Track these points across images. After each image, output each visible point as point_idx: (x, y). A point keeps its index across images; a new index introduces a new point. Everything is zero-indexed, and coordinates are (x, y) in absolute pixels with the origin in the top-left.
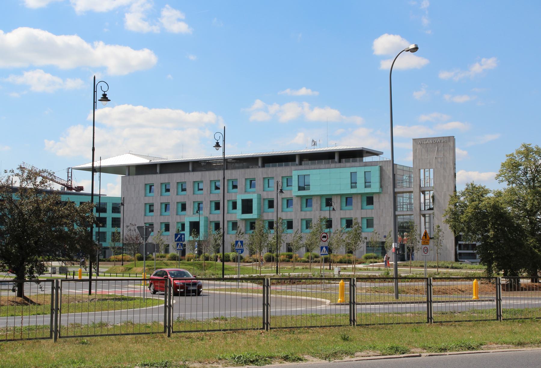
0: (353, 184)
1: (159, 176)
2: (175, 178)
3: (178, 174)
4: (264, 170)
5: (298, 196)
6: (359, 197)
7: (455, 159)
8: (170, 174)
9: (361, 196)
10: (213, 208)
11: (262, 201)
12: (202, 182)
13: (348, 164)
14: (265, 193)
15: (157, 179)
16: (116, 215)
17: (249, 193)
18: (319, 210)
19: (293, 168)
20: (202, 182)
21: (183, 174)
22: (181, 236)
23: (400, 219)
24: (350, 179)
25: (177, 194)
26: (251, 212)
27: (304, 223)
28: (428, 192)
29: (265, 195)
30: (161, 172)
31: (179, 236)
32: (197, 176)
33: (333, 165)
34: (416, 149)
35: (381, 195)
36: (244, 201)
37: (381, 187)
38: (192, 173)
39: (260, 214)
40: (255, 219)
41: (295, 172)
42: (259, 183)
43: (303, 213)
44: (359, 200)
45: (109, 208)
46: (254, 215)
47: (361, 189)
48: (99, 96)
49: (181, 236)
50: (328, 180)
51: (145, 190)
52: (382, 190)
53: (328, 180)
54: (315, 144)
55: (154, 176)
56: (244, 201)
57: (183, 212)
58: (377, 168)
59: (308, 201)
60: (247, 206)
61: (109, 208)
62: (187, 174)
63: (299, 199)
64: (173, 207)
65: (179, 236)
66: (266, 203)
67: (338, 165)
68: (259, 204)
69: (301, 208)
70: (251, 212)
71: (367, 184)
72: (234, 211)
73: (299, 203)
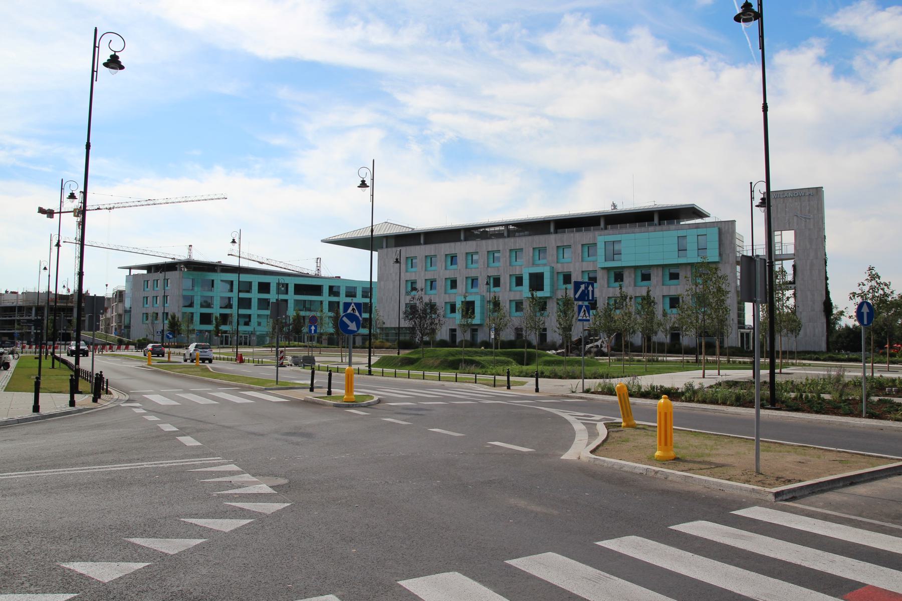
0: (682, 250)
1: (423, 247)
2: (460, 248)
3: (447, 245)
4: (559, 236)
7: (791, 512)
8: (437, 245)
10: (514, 283)
11: (556, 275)
12: (477, 253)
14: (559, 265)
16: (526, 281)
17: (538, 265)
19: (597, 233)
20: (435, 256)
21: (452, 244)
22: (586, 288)
25: (446, 269)
26: (542, 290)
29: (559, 268)
30: (425, 243)
31: (583, 287)
32: (430, 249)
33: (651, 228)
36: (532, 276)
37: (720, 255)
38: (464, 243)
39: (554, 290)
40: (547, 298)
41: (601, 237)
42: (461, 260)
43: (611, 290)
45: (343, 292)
46: (546, 293)
47: (692, 257)
48: (104, 56)
49: (586, 288)
50: (637, 248)
53: (637, 248)
54: (614, 206)
55: (418, 247)
56: (532, 276)
57: (454, 291)
58: (716, 230)
59: (618, 275)
60: (537, 281)
61: (343, 292)
62: (458, 244)
63: (605, 272)
64: (440, 284)
65: (583, 287)
66: (561, 278)
67: (658, 228)
68: (552, 278)
69: (608, 283)
70: (542, 290)
71: (701, 249)
72: (519, 288)
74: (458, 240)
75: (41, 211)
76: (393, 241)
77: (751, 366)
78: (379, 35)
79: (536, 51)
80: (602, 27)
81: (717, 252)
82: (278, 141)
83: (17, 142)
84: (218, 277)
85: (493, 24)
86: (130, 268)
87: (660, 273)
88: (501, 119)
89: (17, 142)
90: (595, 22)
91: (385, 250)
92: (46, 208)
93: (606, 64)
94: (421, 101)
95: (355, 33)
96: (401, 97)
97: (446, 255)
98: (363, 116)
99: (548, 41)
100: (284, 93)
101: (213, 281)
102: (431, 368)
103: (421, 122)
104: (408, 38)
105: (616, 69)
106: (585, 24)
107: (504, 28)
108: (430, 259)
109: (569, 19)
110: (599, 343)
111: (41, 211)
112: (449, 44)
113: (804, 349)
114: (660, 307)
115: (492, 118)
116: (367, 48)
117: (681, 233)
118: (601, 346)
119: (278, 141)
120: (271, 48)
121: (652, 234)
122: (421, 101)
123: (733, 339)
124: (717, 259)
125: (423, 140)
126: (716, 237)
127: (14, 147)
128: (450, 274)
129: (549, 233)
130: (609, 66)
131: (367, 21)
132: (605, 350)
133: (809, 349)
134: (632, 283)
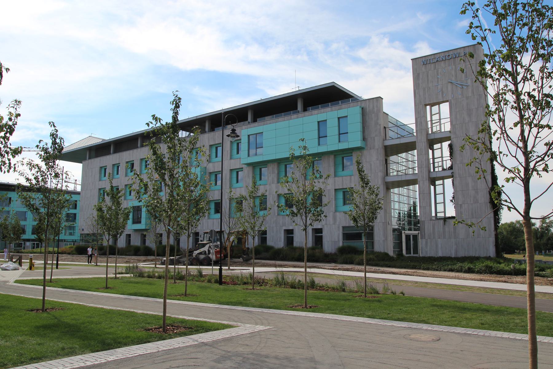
0: (321, 136)
4: (212, 134)
5: (249, 165)
6: (332, 157)
9: (335, 155)
13: (315, 112)
14: (211, 165)
15: (109, 160)
18: (276, 182)
23: (219, 215)
24: (317, 132)
27: (340, 195)
28: (441, 182)
30: (115, 152)
34: (418, 74)
35: (365, 152)
37: (364, 139)
44: (332, 164)
47: (332, 144)
50: (281, 137)
51: (100, 173)
52: (366, 145)
63: (250, 169)
73: (251, 175)
76: (93, 153)
78: (255, 52)
79: (357, 60)
80: (397, 43)
81: (359, 136)
84: (13, 195)
85: (327, 44)
90: (392, 41)
91: (87, 162)
99: (362, 53)
101: (10, 198)
106: (386, 41)
107: (334, 46)
108: (117, 166)
109: (375, 39)
110: (206, 248)
113: (467, 254)
120: (188, 63)
123: (384, 243)
124: (358, 144)
126: (359, 118)
132: (213, 257)
133: (472, 254)
134: (276, 179)
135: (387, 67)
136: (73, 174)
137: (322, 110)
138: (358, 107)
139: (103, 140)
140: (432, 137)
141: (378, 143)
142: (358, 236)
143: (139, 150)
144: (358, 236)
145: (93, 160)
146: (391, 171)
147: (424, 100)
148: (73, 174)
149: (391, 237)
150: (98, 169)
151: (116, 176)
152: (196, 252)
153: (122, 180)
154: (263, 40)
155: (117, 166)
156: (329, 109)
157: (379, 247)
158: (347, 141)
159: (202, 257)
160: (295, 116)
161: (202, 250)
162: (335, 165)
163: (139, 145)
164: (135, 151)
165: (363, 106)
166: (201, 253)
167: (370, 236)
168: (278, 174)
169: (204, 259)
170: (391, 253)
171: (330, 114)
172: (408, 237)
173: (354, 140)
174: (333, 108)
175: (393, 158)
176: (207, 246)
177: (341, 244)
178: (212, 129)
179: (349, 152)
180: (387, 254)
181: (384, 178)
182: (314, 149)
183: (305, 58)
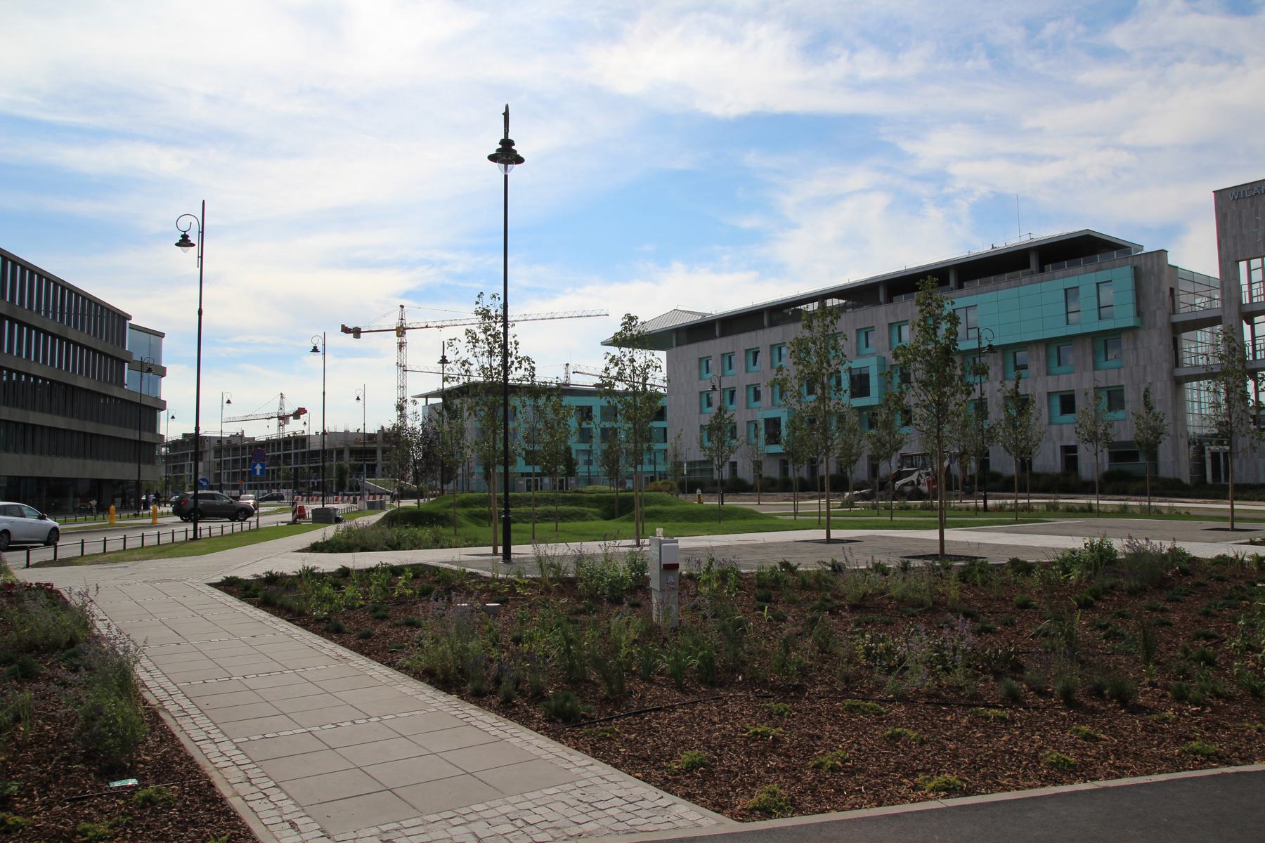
3: (747, 335)
4: (891, 307)
6: (1089, 340)
8: (735, 337)
13: (1060, 273)
15: (714, 347)
17: (864, 356)
25: (747, 371)
26: (867, 394)
30: (723, 335)
35: (1141, 333)
37: (1139, 313)
44: (1089, 351)
47: (1087, 323)
55: (712, 342)
70: (867, 394)
74: (760, 326)
75: (345, 330)
77: (1236, 515)
78: (871, 65)
79: (1104, 54)
81: (1130, 310)
82: (749, 223)
83: (448, 256)
85: (1032, 26)
86: (427, 396)
87: (1042, 354)
88: (1054, 159)
89: (448, 256)
91: (674, 350)
92: (350, 326)
93: (1217, 55)
94: (937, 148)
95: (838, 68)
96: (908, 147)
97: (747, 351)
98: (858, 178)
99: (1119, 36)
100: (752, 158)
102: (71, 514)
103: (939, 177)
104: (912, 63)
105: (1235, 59)
107: (1051, 28)
108: (728, 357)
110: (914, 478)
111: (345, 330)
112: (969, 64)
114: (1042, 414)
115: (1042, 159)
116: (856, 85)
117: (1070, 282)
118: (919, 483)
119: (749, 223)
121: (1025, 290)
122: (937, 148)
123: (1174, 461)
124: (1130, 322)
125: (944, 201)
127: (444, 263)
128: (750, 379)
129: (878, 303)
130: (1226, 57)
131: (853, 50)
132: (925, 489)
135: (1180, 60)
136: (656, 368)
137: (1071, 271)
138: (1128, 268)
139: (704, 315)
140: (1249, 309)
141: (1161, 319)
142: (1133, 456)
143: (767, 331)
144: (1133, 456)
145: (684, 347)
146: (1186, 355)
147: (1232, 249)
148: (656, 368)
149: (1187, 454)
150: (695, 362)
151: (728, 372)
152: (899, 483)
153: (739, 377)
154: (889, 36)
155: (728, 357)
156: (1080, 269)
157: (1165, 471)
158: (1111, 317)
159: (908, 489)
160: (1026, 280)
161: (908, 479)
162: (1094, 352)
163: (766, 323)
164: (760, 332)
165: (1135, 263)
166: (906, 484)
167: (1153, 456)
168: (1004, 366)
169: (912, 492)
170: (1186, 479)
171: (1082, 278)
172: (1215, 456)
173: (1124, 317)
174: (1089, 267)
175: (1185, 335)
176: (916, 474)
177: (1106, 468)
178: (889, 300)
179: (1116, 333)
180: (1178, 481)
181: (1171, 372)
182: (1058, 329)
183: (984, 63)
